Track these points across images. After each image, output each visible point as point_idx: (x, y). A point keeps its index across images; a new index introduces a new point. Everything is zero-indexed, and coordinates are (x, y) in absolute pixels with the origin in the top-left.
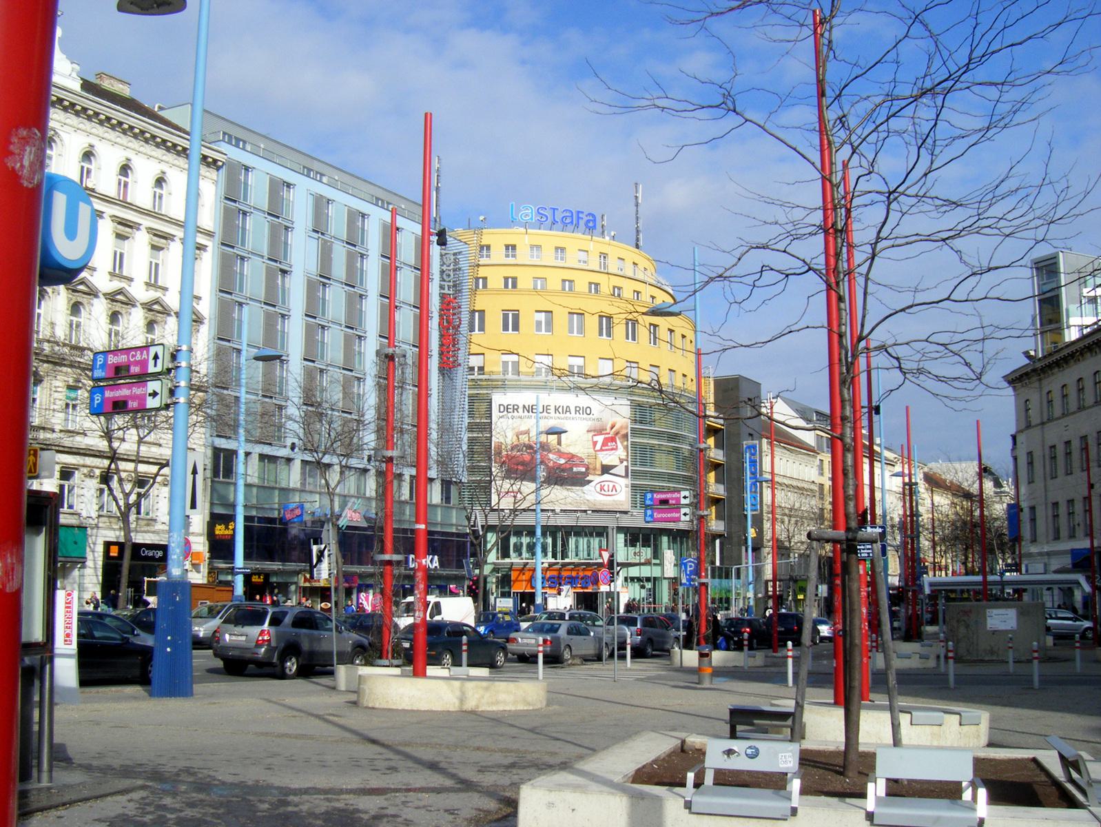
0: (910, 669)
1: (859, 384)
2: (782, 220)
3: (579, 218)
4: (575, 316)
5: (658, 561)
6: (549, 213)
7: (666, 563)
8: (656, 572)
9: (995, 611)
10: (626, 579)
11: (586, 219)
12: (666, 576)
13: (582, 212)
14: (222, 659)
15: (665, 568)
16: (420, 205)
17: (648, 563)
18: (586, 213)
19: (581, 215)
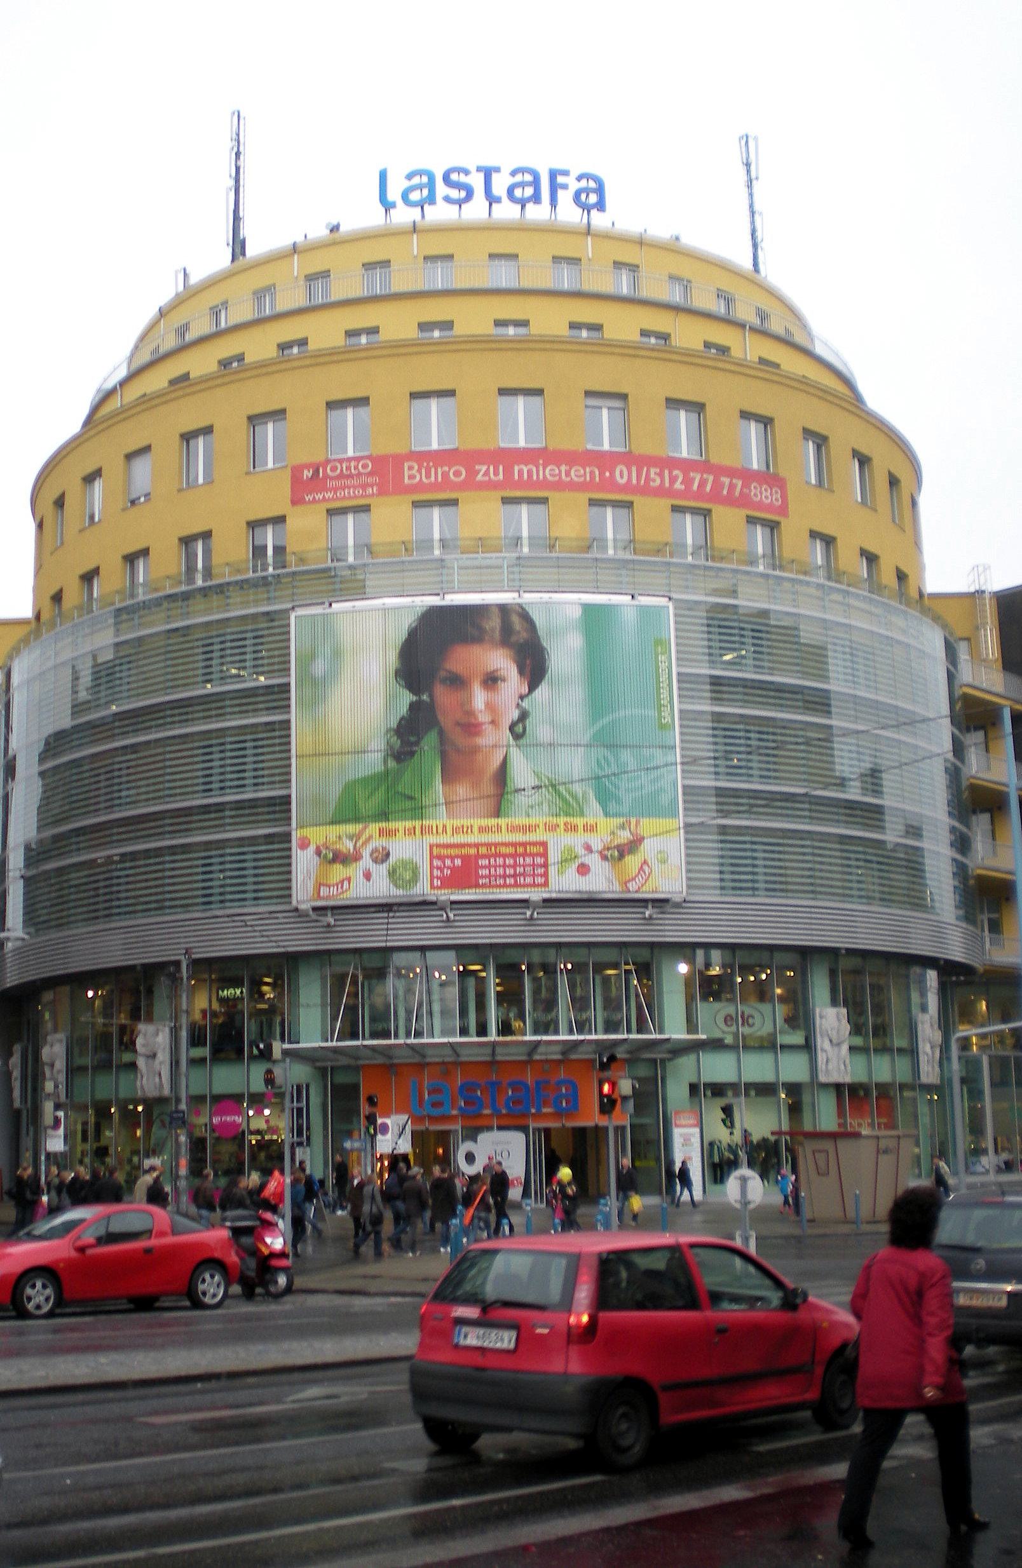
0: (948, 787)
1: (367, 898)
2: (830, 1067)
3: (554, 188)
4: (609, 511)
5: (797, 1038)
6: (476, 181)
7: (822, 1043)
8: (793, 1069)
9: (270, 356)
10: (694, 1088)
11: (574, 186)
12: (823, 1079)
13: (566, 173)
14: (12, 1046)
15: (821, 1058)
16: (238, 246)
17: (769, 1045)
18: (574, 174)
19: (560, 179)
